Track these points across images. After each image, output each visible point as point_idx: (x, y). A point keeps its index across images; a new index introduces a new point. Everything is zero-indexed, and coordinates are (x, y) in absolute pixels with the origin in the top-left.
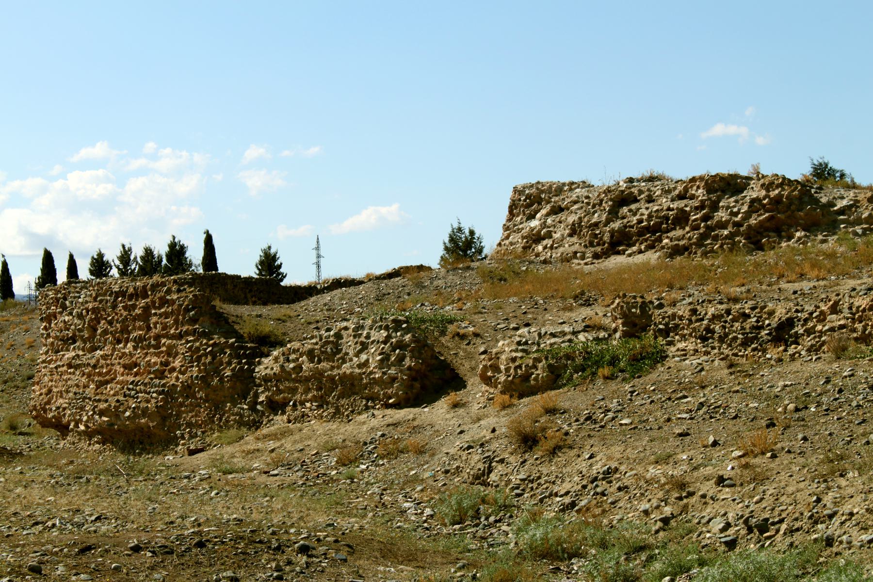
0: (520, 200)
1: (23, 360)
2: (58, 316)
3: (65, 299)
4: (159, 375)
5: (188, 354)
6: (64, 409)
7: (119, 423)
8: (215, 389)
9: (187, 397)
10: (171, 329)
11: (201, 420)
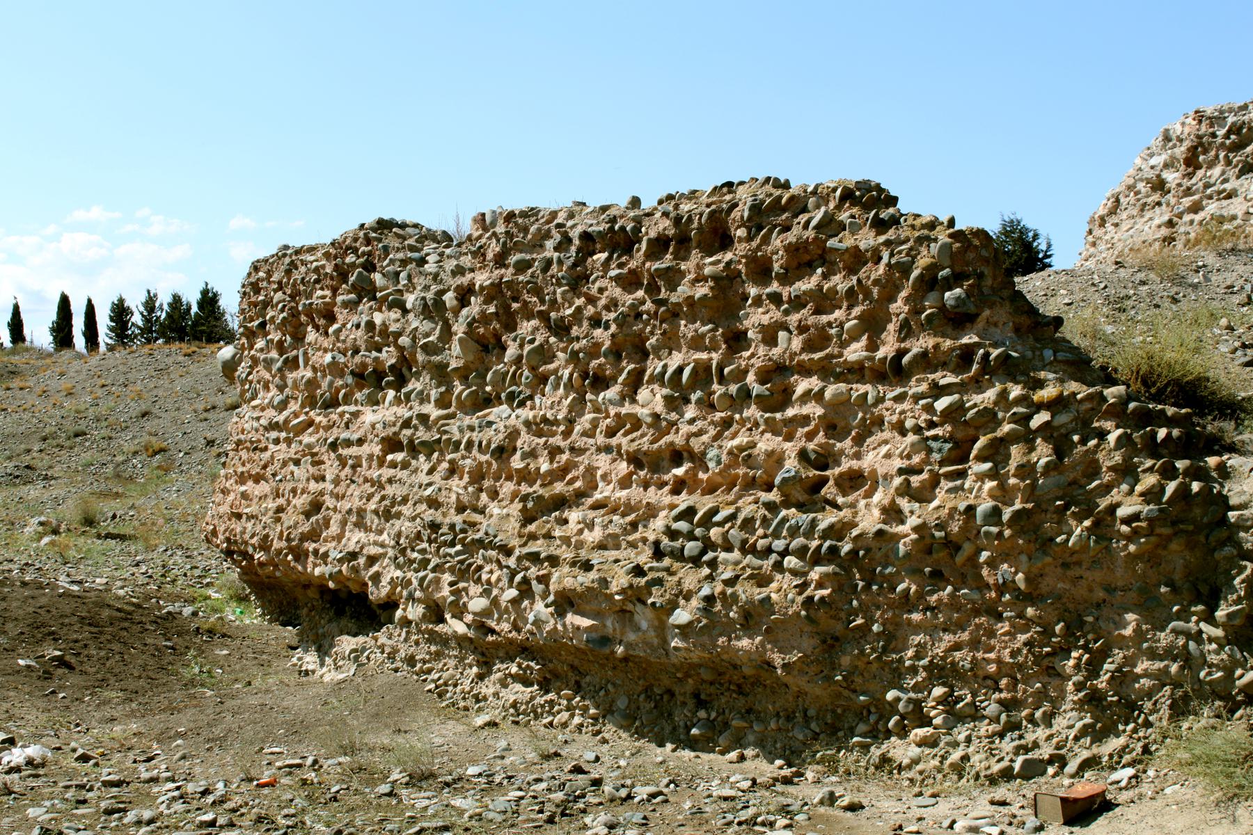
0: (1214, 135)
1: (63, 411)
2: (341, 314)
3: (370, 267)
4: (801, 497)
5: (938, 431)
6: (372, 560)
7: (632, 637)
8: (1069, 561)
9: (938, 577)
10: (844, 345)
11: (999, 661)
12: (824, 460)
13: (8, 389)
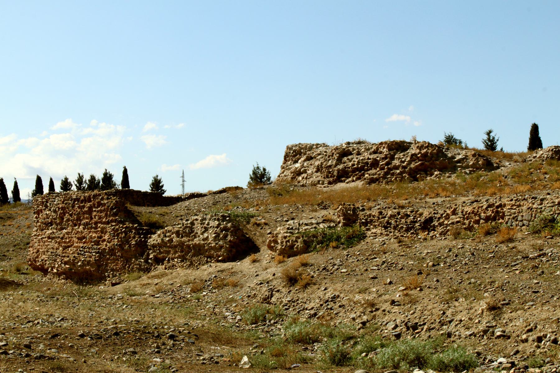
0: (290, 153)
4: (97, 244)
6: (46, 261)
7: (75, 268)
8: (126, 251)
9: (112, 255)
10: (103, 219)
12: (101, 237)
13: (4, 226)
